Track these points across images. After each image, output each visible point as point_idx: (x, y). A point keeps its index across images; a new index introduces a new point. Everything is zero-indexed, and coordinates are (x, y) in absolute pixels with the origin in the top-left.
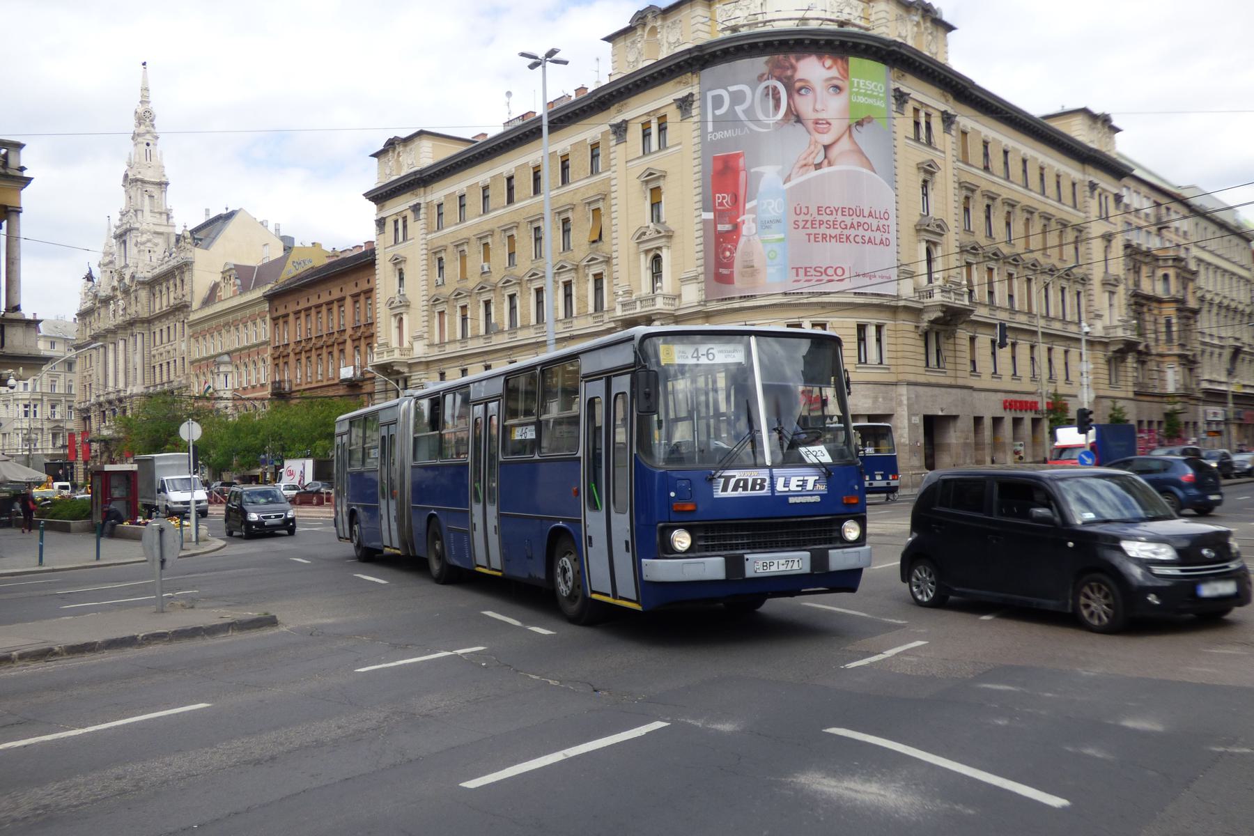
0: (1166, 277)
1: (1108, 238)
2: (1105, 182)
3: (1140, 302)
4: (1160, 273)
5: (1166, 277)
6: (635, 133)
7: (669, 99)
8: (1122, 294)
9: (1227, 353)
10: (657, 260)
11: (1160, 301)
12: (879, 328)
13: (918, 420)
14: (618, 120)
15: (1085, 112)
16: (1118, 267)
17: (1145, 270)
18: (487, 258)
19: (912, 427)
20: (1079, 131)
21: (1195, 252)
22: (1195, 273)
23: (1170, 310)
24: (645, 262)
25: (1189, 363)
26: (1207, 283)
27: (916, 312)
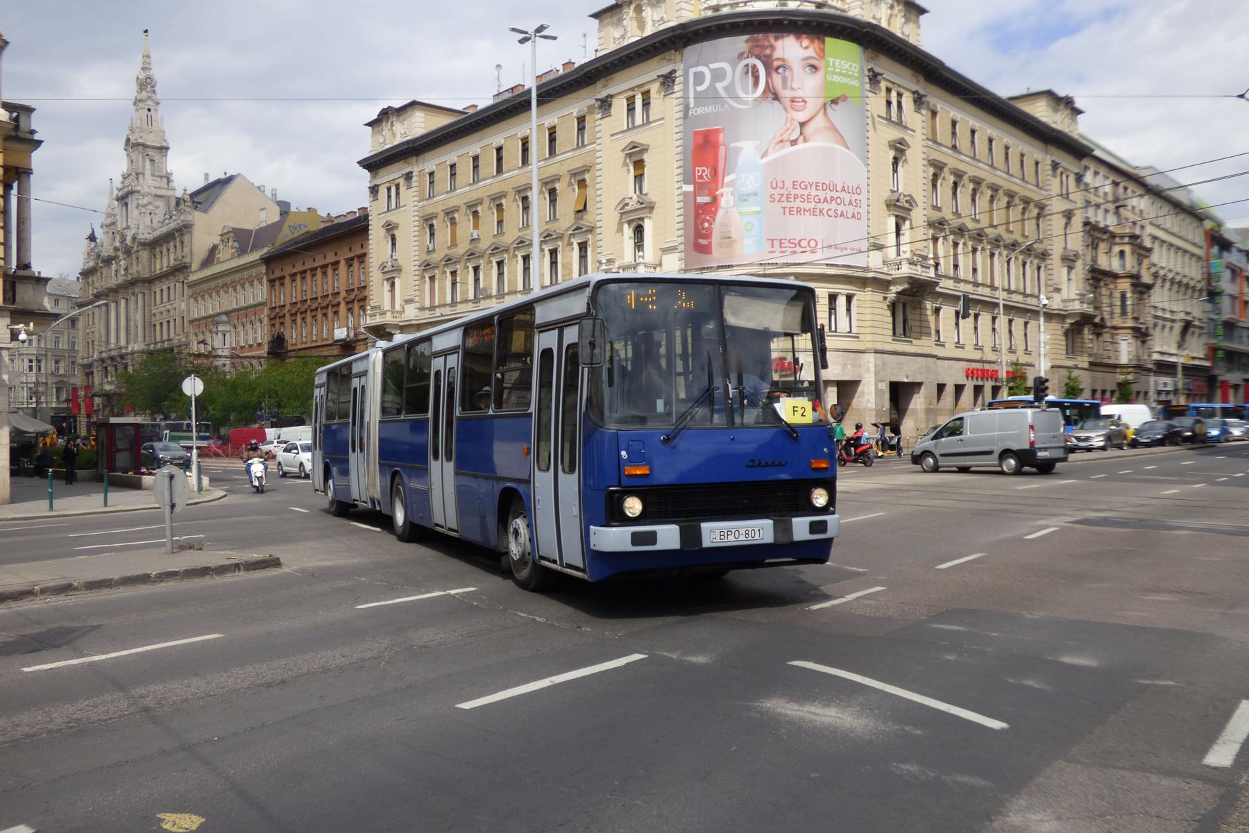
0: (1122, 253)
1: (1068, 215)
2: (1066, 161)
3: (1098, 277)
4: (1117, 249)
5: (1122, 253)
6: (620, 105)
7: (653, 75)
8: (1080, 269)
9: (1178, 327)
10: (639, 231)
11: (1115, 276)
12: (849, 298)
13: (885, 387)
14: (603, 95)
15: (1049, 94)
16: (1076, 241)
17: (1103, 247)
18: (476, 226)
19: (878, 392)
20: (1041, 111)
21: (1150, 230)
22: (1149, 250)
23: (1125, 285)
24: (628, 231)
25: (1141, 335)
26: (1161, 258)
27: (881, 284)
